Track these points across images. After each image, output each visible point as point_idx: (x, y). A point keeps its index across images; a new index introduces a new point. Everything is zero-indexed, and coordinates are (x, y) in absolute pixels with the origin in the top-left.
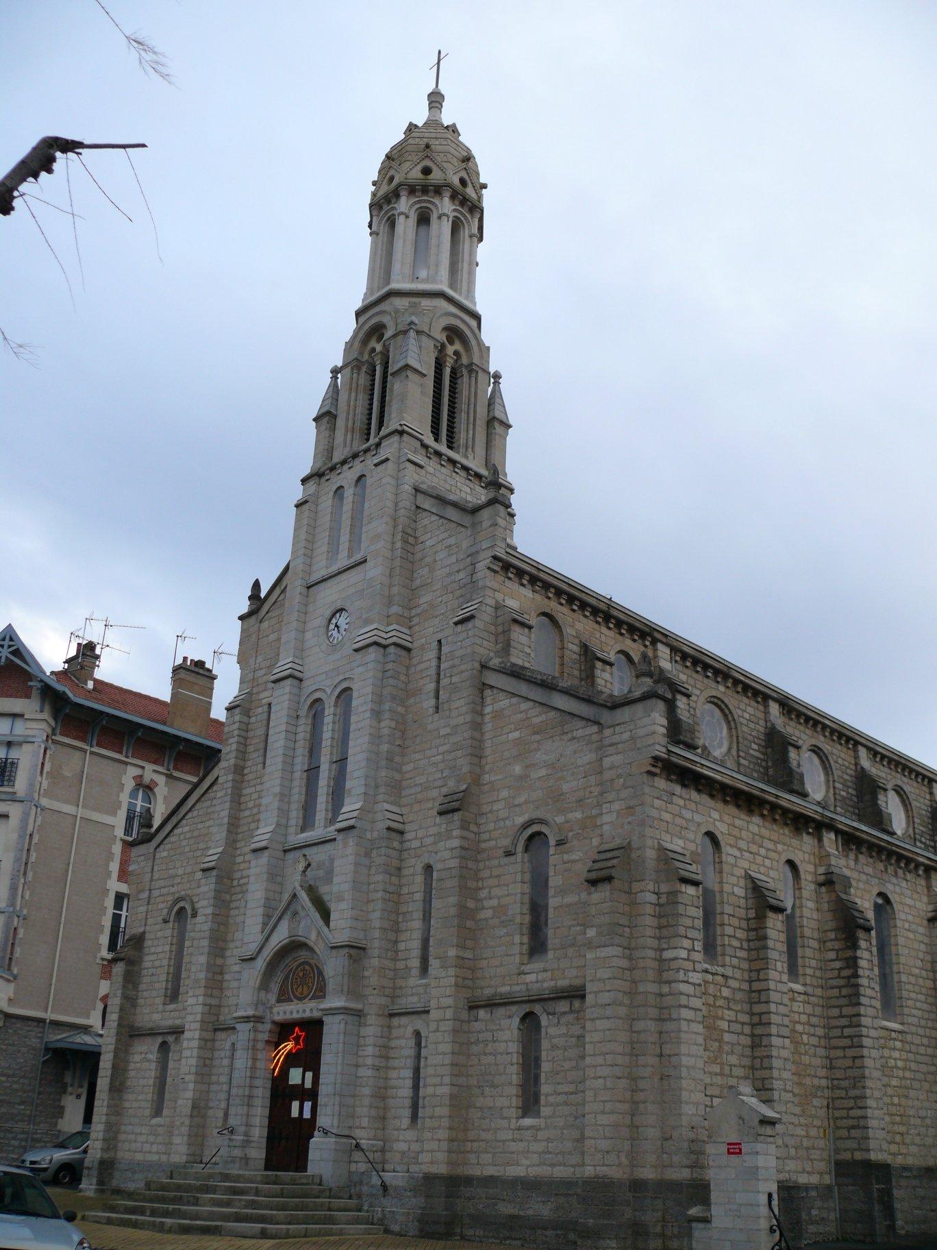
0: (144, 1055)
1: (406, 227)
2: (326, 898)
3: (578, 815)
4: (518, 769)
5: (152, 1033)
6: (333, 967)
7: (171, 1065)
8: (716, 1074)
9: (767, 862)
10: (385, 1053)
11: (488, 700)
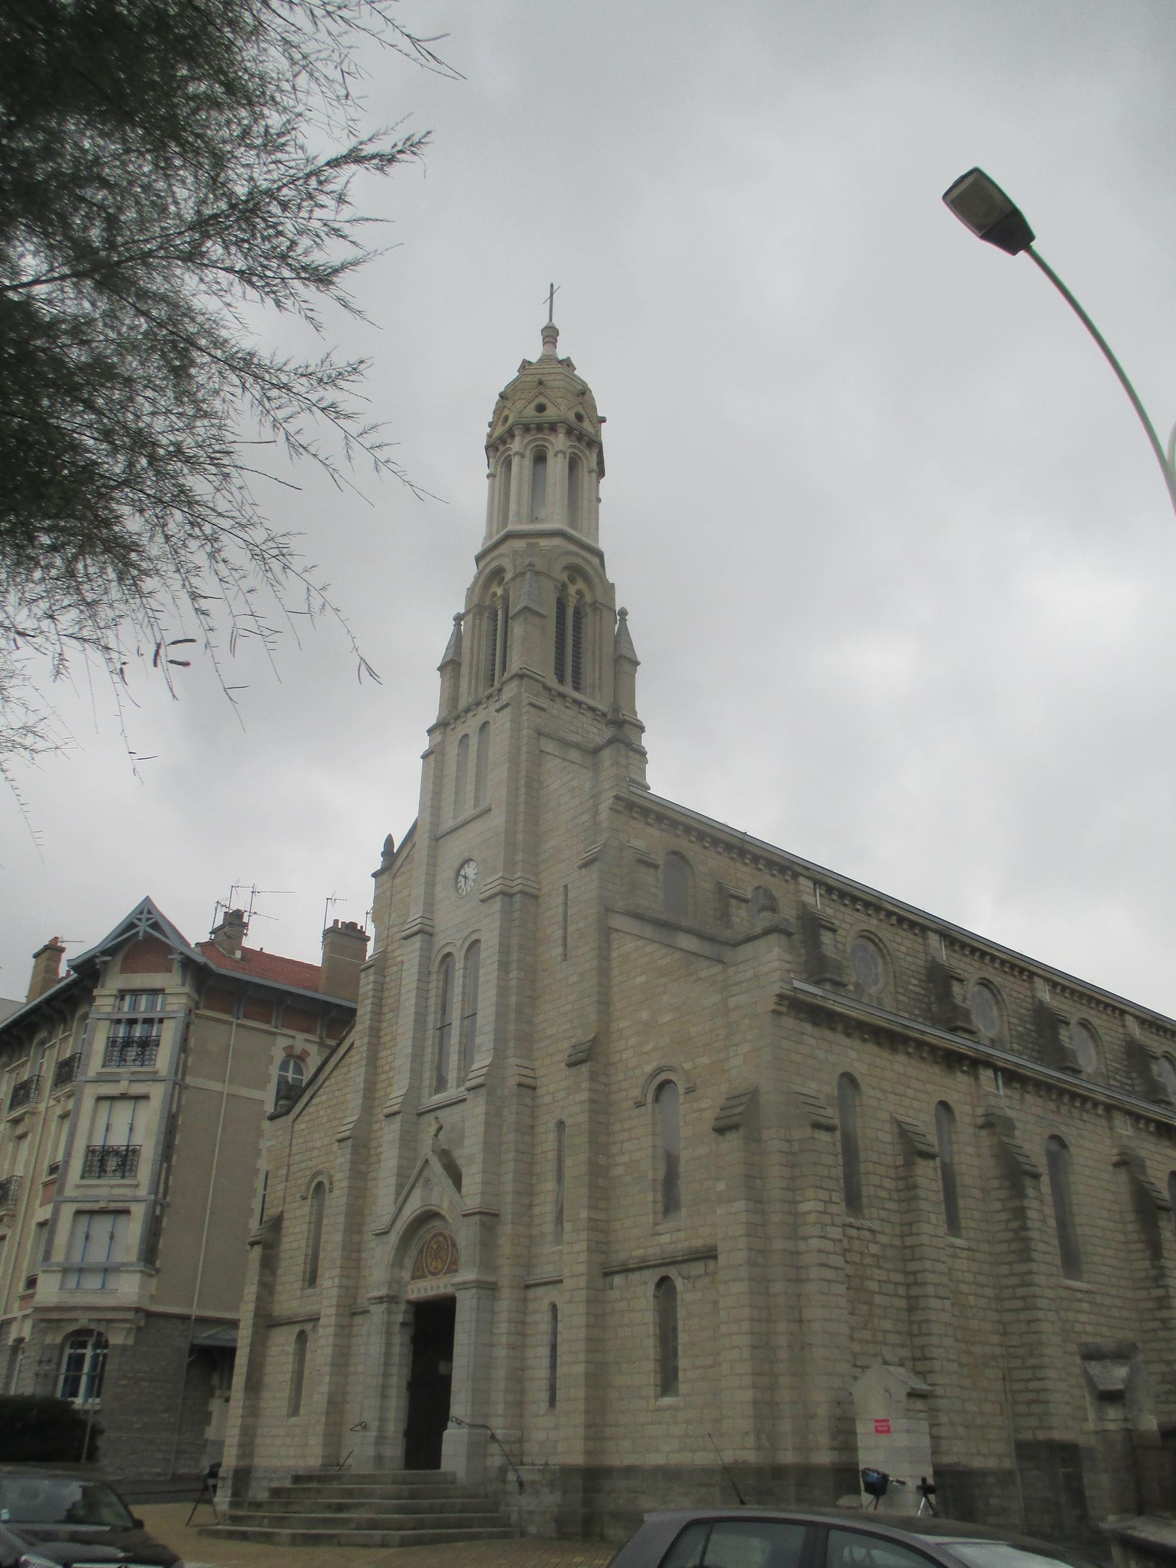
0: (282, 1342)
1: (521, 468)
2: (459, 1162)
3: (705, 1060)
4: (644, 1015)
5: (290, 1322)
6: (466, 1235)
7: (308, 1357)
8: (868, 1342)
9: (916, 1104)
10: (521, 1327)
11: (615, 945)
